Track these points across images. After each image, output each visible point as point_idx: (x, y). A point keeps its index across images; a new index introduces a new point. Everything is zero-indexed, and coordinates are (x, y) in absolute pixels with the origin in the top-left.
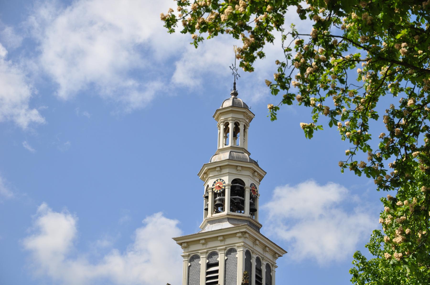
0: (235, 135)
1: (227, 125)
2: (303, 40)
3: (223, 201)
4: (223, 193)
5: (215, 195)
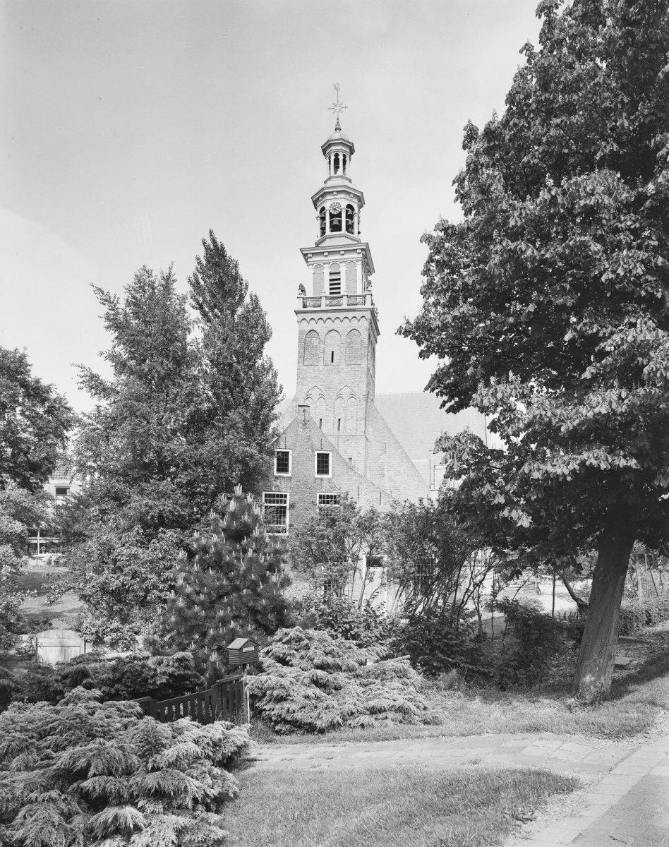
0: (337, 167)
1: (337, 155)
2: (23, 358)
3: (340, 222)
4: (339, 215)
5: (332, 216)
